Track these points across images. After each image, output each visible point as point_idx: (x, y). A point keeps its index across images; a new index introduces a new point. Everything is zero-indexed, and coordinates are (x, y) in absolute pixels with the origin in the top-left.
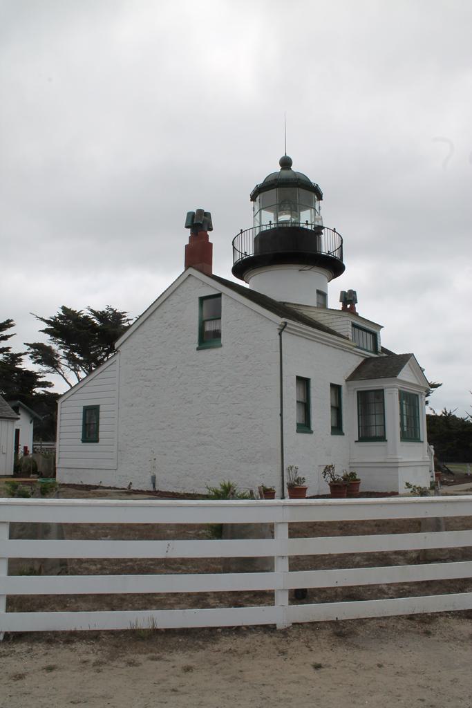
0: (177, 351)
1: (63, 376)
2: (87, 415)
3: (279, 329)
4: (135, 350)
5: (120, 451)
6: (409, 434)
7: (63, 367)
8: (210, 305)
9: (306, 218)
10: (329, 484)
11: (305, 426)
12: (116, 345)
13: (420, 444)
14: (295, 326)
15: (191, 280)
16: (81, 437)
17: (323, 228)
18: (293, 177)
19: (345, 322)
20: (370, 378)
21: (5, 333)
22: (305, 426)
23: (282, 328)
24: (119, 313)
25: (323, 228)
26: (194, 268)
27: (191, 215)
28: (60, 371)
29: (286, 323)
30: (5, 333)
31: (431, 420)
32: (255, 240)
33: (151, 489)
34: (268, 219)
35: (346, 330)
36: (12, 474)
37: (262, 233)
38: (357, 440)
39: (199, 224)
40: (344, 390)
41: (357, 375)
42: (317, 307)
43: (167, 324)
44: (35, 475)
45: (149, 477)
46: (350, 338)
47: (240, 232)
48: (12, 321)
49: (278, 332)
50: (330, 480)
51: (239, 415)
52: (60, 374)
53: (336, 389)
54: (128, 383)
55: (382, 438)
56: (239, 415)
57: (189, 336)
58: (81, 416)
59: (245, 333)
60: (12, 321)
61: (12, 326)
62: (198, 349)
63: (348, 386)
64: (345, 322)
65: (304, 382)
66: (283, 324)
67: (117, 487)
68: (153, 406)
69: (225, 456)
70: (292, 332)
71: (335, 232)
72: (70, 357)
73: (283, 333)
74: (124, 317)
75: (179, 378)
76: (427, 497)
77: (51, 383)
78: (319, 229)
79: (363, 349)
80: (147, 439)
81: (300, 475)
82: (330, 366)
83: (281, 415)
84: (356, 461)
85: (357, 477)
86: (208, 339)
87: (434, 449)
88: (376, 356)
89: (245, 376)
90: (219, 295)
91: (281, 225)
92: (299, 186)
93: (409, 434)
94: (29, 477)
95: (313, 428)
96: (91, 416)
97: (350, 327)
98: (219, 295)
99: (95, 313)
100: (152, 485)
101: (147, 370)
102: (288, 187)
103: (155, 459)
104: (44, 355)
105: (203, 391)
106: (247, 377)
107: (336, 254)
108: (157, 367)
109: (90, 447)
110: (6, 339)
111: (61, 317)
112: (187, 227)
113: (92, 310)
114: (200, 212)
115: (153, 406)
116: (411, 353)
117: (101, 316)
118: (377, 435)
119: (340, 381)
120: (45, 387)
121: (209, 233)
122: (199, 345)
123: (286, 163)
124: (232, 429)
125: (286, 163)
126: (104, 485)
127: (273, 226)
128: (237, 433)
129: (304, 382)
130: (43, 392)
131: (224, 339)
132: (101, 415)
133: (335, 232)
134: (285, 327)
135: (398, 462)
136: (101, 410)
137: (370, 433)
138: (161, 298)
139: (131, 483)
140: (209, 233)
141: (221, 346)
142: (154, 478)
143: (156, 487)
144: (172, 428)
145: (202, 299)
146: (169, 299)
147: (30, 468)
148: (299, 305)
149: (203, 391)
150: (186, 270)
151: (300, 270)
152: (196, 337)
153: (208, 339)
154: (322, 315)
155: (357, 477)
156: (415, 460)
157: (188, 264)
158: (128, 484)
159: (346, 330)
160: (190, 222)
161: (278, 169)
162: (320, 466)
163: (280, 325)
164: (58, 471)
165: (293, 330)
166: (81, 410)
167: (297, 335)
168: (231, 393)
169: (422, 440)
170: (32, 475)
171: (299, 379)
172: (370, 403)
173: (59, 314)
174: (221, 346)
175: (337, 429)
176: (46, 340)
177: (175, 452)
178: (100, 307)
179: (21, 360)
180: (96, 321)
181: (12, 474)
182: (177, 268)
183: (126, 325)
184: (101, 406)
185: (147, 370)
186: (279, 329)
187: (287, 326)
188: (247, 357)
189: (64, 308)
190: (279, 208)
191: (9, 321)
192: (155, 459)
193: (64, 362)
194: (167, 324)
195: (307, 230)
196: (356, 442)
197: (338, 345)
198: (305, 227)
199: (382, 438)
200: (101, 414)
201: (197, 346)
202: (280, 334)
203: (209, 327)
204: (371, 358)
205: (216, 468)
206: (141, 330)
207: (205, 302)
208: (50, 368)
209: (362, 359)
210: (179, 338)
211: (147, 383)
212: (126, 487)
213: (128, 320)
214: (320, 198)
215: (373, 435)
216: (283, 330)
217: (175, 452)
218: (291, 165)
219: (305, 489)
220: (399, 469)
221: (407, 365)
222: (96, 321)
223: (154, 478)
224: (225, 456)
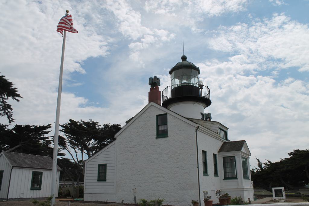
0: (146, 139)
1: (68, 150)
2: (100, 168)
3: (195, 129)
4: (125, 138)
5: (117, 185)
6: (246, 177)
7: (68, 146)
8: (162, 120)
9: (194, 81)
10: (219, 199)
11: (206, 172)
12: (115, 136)
13: (249, 180)
14: (202, 128)
15: (152, 107)
16: (97, 179)
17: (203, 86)
18: (189, 64)
19: (216, 127)
20: (229, 151)
21: (47, 130)
22: (206, 172)
23: (197, 129)
24: (95, 123)
25: (203, 86)
26: (154, 102)
27: (151, 79)
28: (67, 149)
29: (198, 126)
30: (47, 130)
31: (41, 173)
32: (172, 91)
33: (134, 203)
34: (177, 82)
35: (216, 130)
36: (58, 197)
37: (176, 88)
38: (224, 179)
39: (154, 83)
40: (217, 156)
41: (221, 150)
42: (201, 120)
43: (141, 127)
44: (69, 197)
45: (132, 197)
46: (218, 133)
47: (167, 87)
48: (51, 125)
49: (195, 130)
50: (219, 197)
51: (178, 168)
52: (67, 150)
53: (215, 155)
54: (121, 154)
55: (236, 178)
56: (178, 168)
57: (152, 132)
58: (97, 169)
59: (179, 131)
60: (51, 125)
61: (51, 127)
62: (156, 138)
63: (219, 155)
64: (216, 127)
65: (204, 152)
66: (197, 127)
67: (116, 202)
68: (134, 164)
69: (171, 187)
70: (200, 131)
71: (208, 88)
72: (71, 142)
73: (197, 131)
74: (97, 124)
75: (147, 151)
76: (292, 203)
77: (64, 154)
78: (201, 86)
79: (222, 138)
80: (131, 179)
81: (209, 195)
82: (212, 146)
83: (198, 168)
84: (223, 188)
85: (229, 196)
86: (162, 134)
87: (253, 183)
88: (227, 141)
89: (180, 150)
90: (166, 114)
91: (182, 85)
92: (191, 68)
93: (246, 177)
94: (66, 198)
95: (208, 173)
96: (102, 169)
97: (218, 128)
98: (166, 114)
99: (85, 123)
100: (134, 201)
101: (131, 148)
102: (185, 68)
103: (135, 189)
104: (62, 142)
105: (159, 157)
106: (181, 151)
107: (207, 97)
108: (136, 146)
109: (249, 198)
110: (48, 133)
111: (69, 124)
112: (149, 84)
113: (83, 121)
114: (155, 77)
115: (134, 164)
116: (244, 140)
117: (87, 124)
118: (229, 177)
119: (216, 153)
120: (61, 156)
121: (159, 87)
122: (157, 136)
123: (184, 58)
124: (174, 174)
125: (184, 58)
126: (109, 201)
127: (179, 85)
128: (177, 176)
129: (204, 152)
130: (62, 159)
131: (169, 133)
132: (108, 168)
133: (208, 88)
134: (198, 128)
135: (244, 189)
136: (107, 166)
137: (230, 176)
138: (138, 114)
139: (123, 200)
140: (159, 87)
141: (168, 137)
142: (135, 198)
143: (136, 202)
144: (144, 174)
145: (157, 116)
146: (141, 116)
147: (66, 193)
148: (194, 119)
149: (159, 157)
150: (149, 103)
151: (194, 104)
152: (155, 133)
153: (162, 134)
154: (205, 123)
155: (229, 196)
156: (246, 188)
157: (150, 101)
158: (122, 201)
159: (216, 130)
160: (151, 82)
161: (181, 61)
162: (211, 191)
163: (196, 128)
164: (84, 195)
165: (203, 131)
166: (97, 166)
167: (202, 132)
168: (173, 158)
169: (249, 178)
170: (68, 197)
171: (203, 151)
172: (229, 162)
173: (68, 123)
174: (168, 137)
175: (216, 174)
176: (62, 134)
177: (146, 185)
178: (87, 120)
179: (51, 143)
180: (85, 126)
181: (58, 197)
182: (146, 102)
183: (98, 128)
184: (107, 164)
185: (131, 148)
186: (195, 129)
187: (199, 128)
188: (181, 142)
189: (71, 120)
190: (180, 78)
191: (49, 125)
192: (135, 189)
193: (69, 144)
194: (141, 127)
195: (195, 86)
196: (223, 179)
197: (215, 136)
198: (194, 85)
199: (236, 178)
200: (107, 168)
201: (156, 137)
202: (196, 131)
203: (161, 128)
204: (226, 142)
205: (167, 193)
206: (127, 129)
207: (159, 117)
208: (62, 147)
209: (222, 143)
210: (147, 133)
211: (131, 154)
212: (120, 202)
213: (99, 126)
214: (199, 73)
215: (228, 177)
216: (197, 130)
217: (146, 185)
218: (186, 59)
219: (212, 201)
220: (244, 191)
221: (243, 147)
222: (85, 126)
223: (135, 198)
224: (171, 187)
